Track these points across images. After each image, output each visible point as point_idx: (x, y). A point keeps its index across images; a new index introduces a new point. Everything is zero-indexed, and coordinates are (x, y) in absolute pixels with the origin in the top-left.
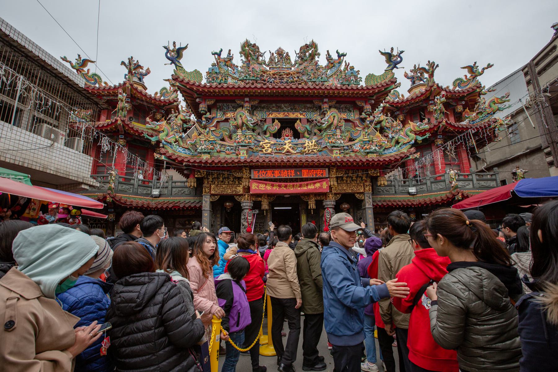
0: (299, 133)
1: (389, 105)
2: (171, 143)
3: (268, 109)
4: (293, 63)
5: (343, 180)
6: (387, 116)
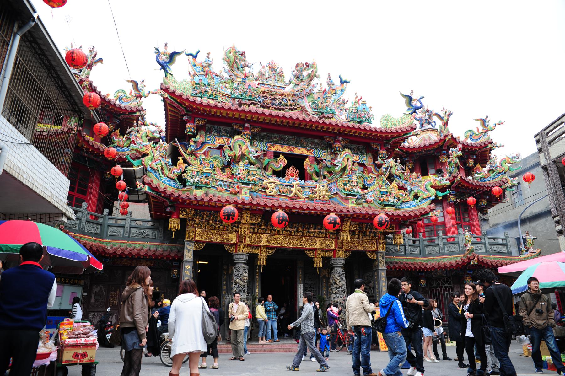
3: (269, 139)
4: (287, 81)
6: (396, 161)
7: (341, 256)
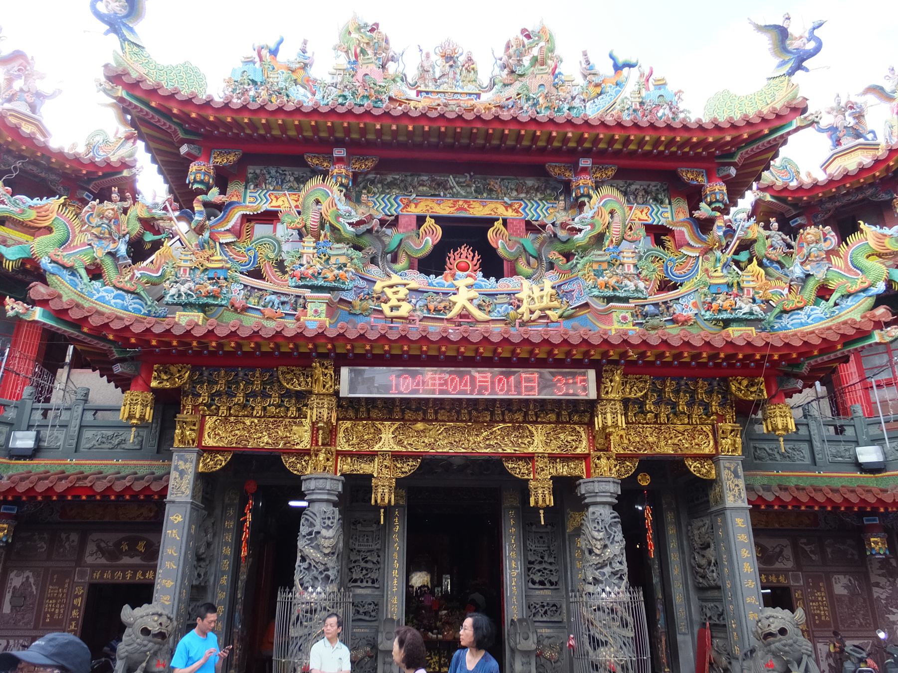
0: (499, 261)
1: (772, 196)
3: (406, 188)
4: (486, 82)
5: (645, 413)
6: (767, 227)
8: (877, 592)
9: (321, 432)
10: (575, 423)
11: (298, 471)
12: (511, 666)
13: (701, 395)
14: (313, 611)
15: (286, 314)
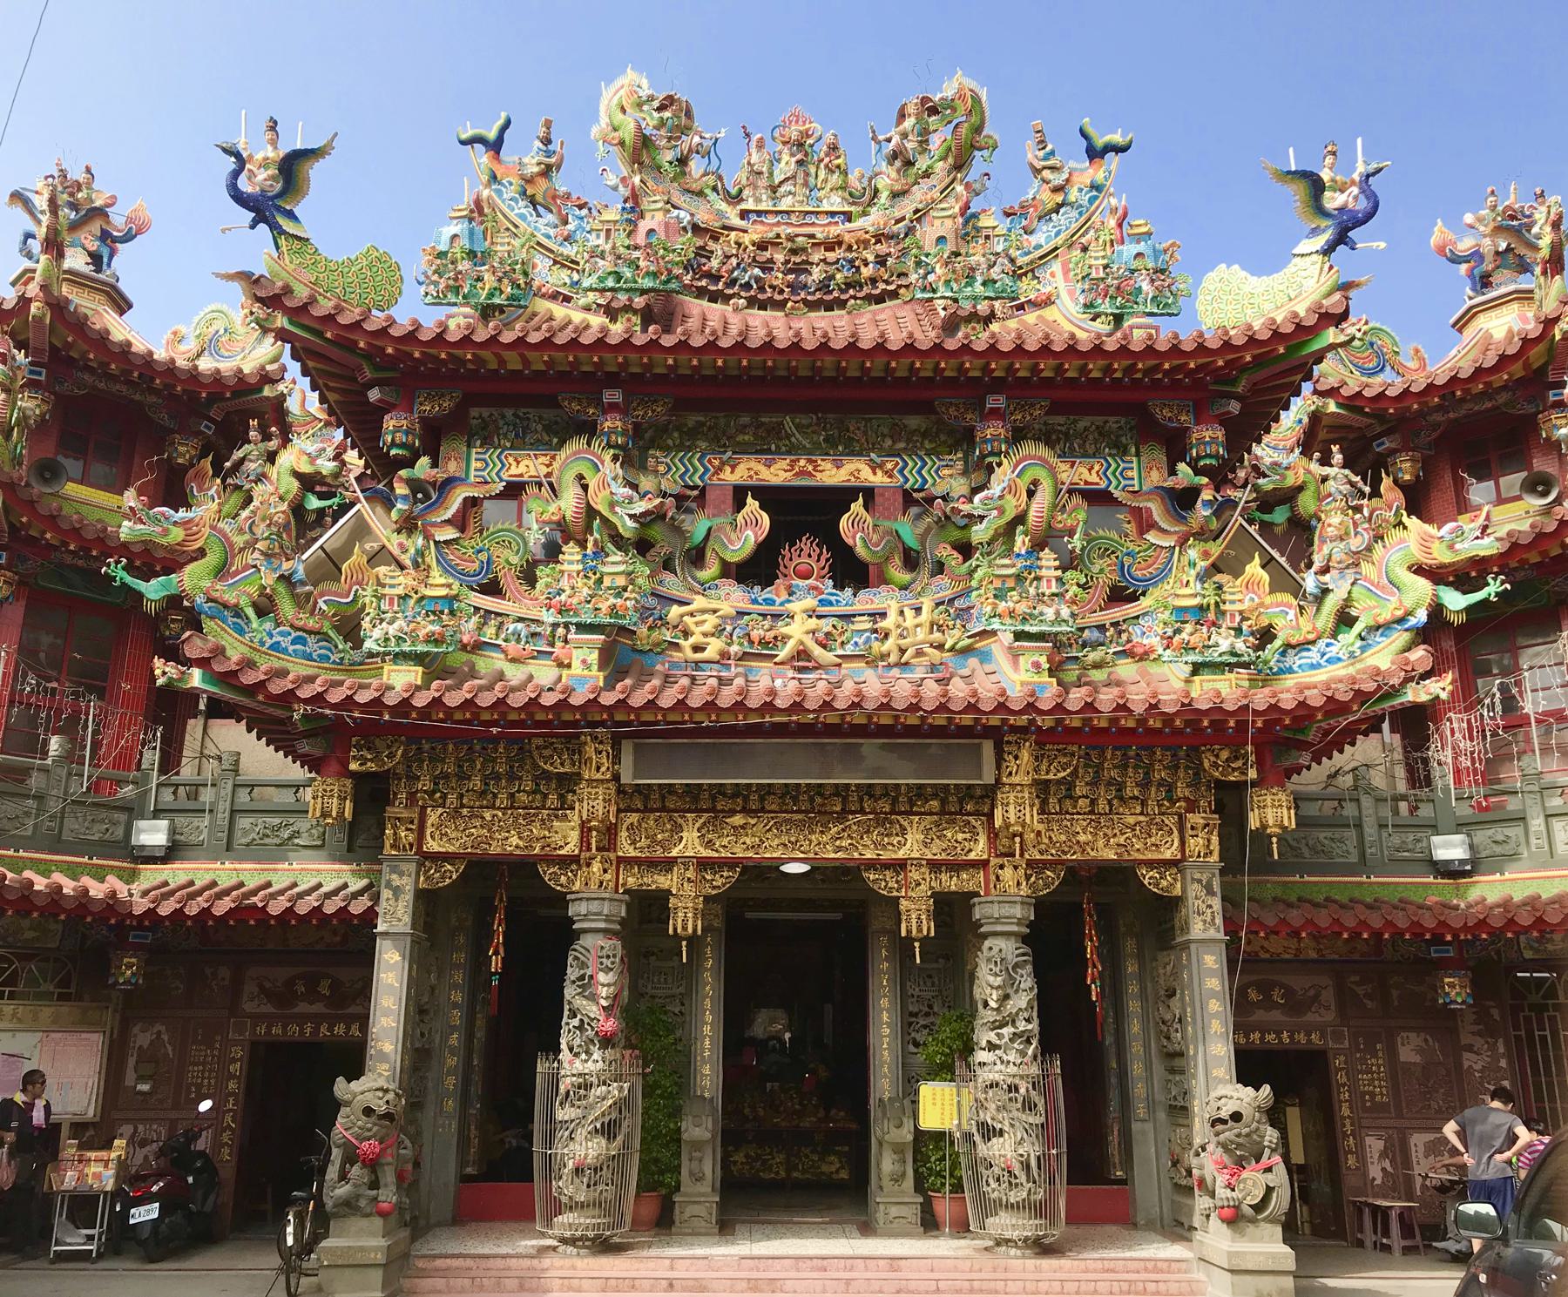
1: (1339, 405)
2: (237, 612)
3: (716, 440)
6: (1326, 461)
7: (1013, 890)
8: (1468, 1060)
9: (594, 833)
10: (969, 814)
11: (562, 885)
12: (879, 1163)
13: (1160, 774)
14: (588, 1086)
15: (538, 652)
